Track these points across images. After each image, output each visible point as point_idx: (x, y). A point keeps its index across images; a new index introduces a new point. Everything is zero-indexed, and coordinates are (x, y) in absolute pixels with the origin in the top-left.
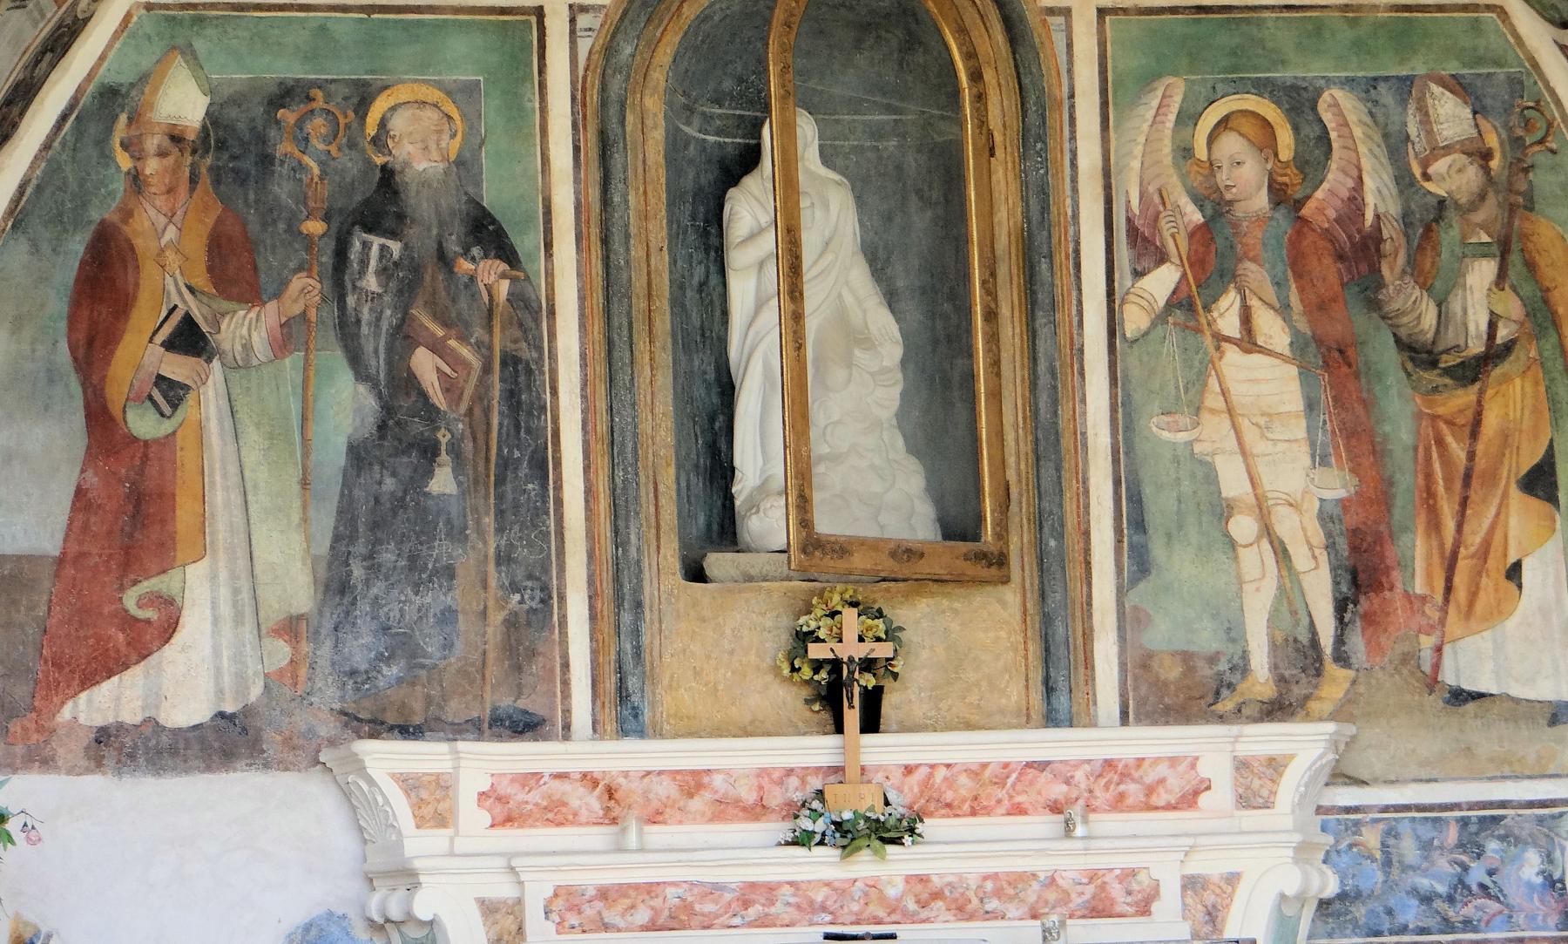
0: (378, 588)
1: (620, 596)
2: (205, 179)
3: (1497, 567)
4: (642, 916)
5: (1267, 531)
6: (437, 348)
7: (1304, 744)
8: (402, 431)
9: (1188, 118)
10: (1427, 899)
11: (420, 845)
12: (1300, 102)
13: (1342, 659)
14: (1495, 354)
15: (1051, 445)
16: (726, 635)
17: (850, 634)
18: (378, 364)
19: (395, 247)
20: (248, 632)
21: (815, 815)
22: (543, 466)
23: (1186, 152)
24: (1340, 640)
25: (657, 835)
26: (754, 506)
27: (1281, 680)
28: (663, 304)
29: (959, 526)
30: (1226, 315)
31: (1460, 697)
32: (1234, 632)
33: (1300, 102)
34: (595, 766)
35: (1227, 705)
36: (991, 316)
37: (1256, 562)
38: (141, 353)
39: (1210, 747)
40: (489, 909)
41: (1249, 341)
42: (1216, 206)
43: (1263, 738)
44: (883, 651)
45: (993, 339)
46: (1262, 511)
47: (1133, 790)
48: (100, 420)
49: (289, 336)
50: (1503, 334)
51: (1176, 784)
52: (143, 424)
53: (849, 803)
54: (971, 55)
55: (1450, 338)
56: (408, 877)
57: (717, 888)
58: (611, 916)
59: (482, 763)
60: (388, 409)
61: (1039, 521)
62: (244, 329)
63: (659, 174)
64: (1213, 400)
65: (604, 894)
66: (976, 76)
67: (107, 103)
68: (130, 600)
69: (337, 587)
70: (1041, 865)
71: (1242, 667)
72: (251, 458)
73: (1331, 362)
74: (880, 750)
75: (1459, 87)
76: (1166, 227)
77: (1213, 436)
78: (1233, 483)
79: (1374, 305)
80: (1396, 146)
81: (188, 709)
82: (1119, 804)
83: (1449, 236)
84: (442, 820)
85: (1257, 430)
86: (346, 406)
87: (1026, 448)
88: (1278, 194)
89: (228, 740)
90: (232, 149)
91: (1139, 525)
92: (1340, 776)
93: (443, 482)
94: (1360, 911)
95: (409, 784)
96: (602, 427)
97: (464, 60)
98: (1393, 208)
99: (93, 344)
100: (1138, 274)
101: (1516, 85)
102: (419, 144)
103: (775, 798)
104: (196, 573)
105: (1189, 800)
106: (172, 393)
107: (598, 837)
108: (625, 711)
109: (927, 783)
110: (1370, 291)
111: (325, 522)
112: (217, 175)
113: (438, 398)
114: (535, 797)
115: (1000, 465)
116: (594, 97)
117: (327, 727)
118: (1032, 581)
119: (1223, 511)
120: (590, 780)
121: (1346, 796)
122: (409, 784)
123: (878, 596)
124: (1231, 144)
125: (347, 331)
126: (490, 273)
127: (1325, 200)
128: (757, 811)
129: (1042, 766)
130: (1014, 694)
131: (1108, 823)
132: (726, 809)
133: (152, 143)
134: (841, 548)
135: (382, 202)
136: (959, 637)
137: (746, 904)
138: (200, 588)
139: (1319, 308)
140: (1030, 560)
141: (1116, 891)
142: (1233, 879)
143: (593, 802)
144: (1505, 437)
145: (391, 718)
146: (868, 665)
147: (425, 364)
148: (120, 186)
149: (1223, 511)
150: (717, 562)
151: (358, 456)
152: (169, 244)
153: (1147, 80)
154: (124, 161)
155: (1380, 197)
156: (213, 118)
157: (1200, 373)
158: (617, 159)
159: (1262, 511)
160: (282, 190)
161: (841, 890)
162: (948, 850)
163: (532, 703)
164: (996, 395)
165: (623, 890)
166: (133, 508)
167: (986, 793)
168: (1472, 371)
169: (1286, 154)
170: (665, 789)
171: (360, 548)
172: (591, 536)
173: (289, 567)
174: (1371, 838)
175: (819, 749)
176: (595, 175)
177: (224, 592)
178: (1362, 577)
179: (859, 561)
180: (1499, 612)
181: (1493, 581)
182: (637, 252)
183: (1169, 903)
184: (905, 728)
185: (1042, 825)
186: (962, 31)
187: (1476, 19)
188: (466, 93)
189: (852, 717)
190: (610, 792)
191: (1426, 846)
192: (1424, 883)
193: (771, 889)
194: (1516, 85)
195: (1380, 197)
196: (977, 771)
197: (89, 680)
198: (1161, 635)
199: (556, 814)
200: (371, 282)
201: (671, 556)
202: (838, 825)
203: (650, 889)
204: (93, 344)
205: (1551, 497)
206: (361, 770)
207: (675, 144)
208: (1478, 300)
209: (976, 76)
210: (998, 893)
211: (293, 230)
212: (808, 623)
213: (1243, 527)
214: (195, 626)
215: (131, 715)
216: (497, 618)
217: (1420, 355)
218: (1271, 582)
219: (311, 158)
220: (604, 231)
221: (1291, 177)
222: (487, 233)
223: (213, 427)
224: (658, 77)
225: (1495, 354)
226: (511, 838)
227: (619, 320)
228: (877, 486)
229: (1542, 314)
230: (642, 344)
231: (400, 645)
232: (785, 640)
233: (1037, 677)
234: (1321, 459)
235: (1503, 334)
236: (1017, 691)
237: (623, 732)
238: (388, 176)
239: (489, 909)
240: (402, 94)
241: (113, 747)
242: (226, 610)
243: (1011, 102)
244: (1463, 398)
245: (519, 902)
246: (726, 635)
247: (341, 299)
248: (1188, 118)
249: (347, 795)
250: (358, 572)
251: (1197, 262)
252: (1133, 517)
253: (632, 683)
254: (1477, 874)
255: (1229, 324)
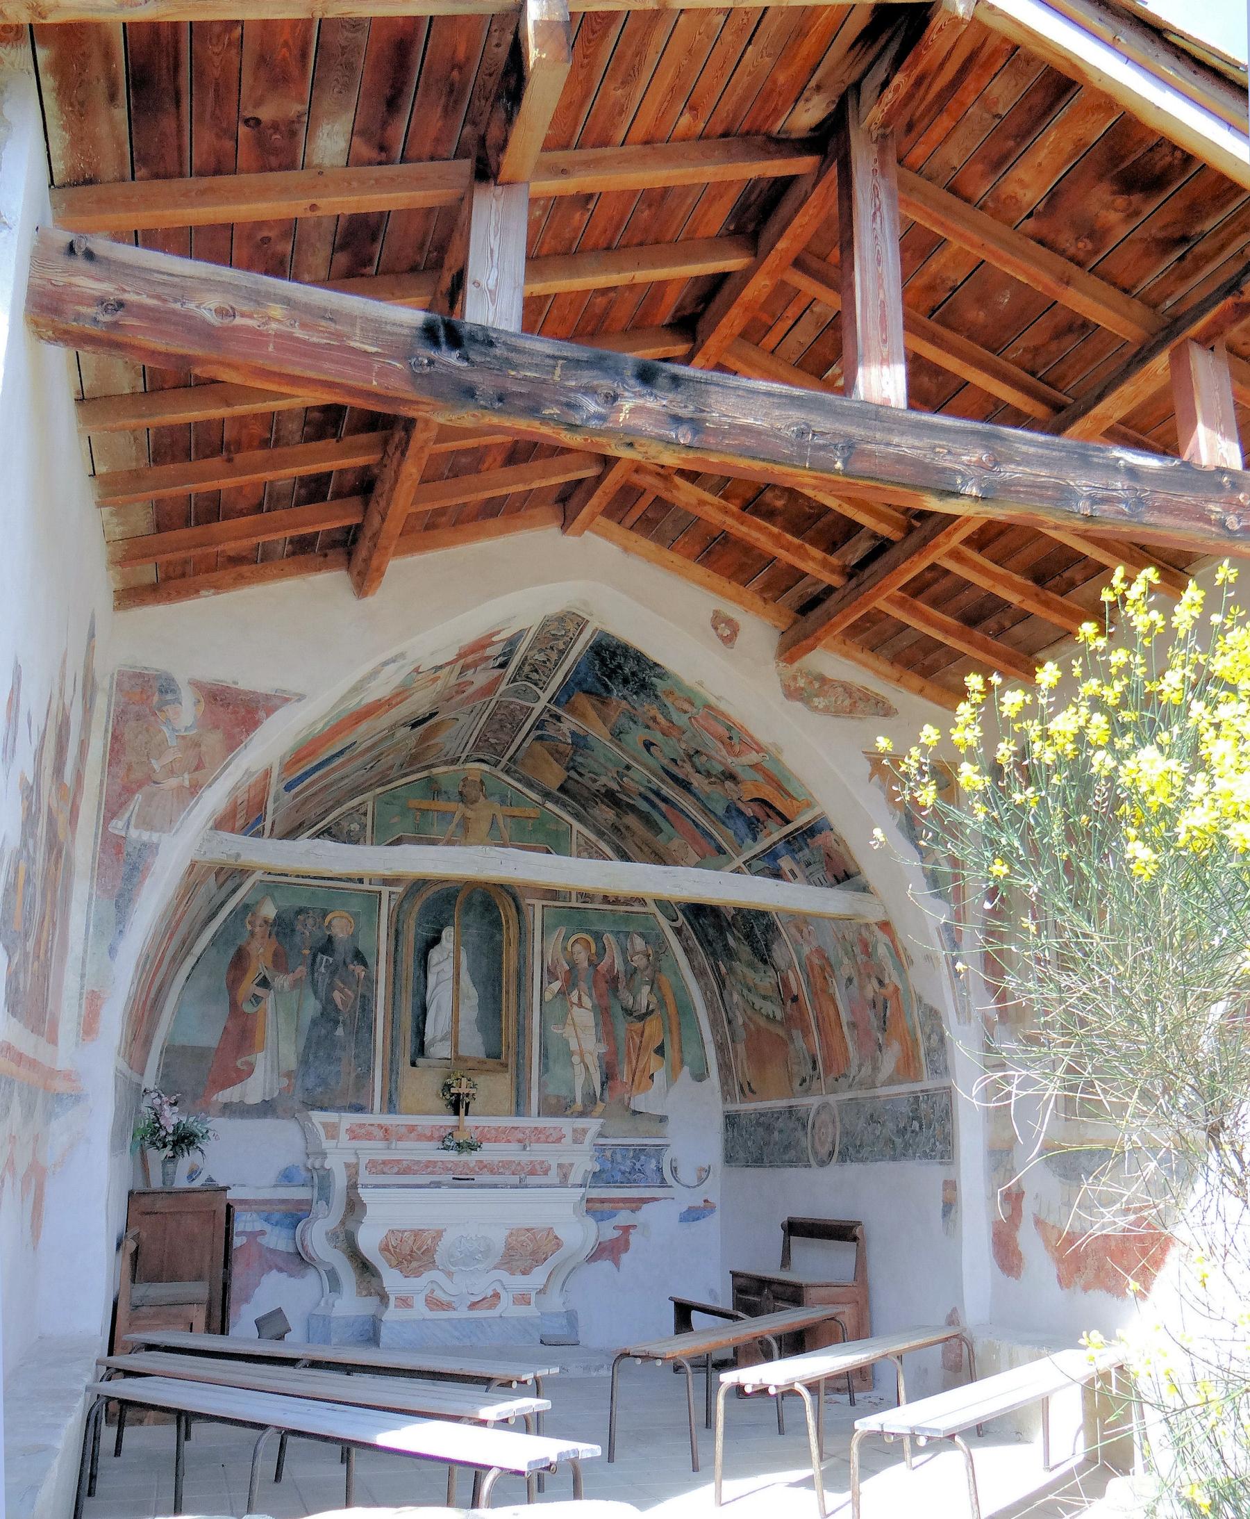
0: (317, 1063)
1: (392, 1070)
2: (273, 936)
3: (647, 1075)
4: (396, 1169)
5: (583, 1061)
6: (341, 991)
7: (592, 1125)
8: (329, 1015)
9: (566, 938)
10: (623, 1173)
11: (327, 1144)
12: (598, 936)
13: (602, 1100)
14: (649, 1013)
15: (522, 1032)
16: (422, 1084)
17: (464, 1085)
18: (323, 994)
19: (331, 960)
20: (275, 1076)
21: (451, 1141)
22: (371, 1029)
23: (566, 949)
24: (602, 1094)
25: (401, 1144)
26: (432, 1044)
27: (585, 1106)
28: (411, 982)
29: (494, 1055)
30: (574, 997)
31: (635, 1113)
32: (572, 1090)
33: (598, 936)
34: (382, 1122)
35: (568, 1112)
36: (507, 992)
37: (579, 1069)
38: (249, 986)
39: (566, 1124)
40: (347, 1166)
41: (580, 1005)
42: (573, 966)
43: (581, 1123)
44: (473, 1091)
45: (508, 999)
46: (582, 1056)
47: (543, 1137)
48: (234, 1006)
49: (295, 984)
50: (651, 1007)
51: (555, 1136)
52: (248, 1008)
53: (461, 1137)
54: (506, 916)
55: (637, 1007)
56: (324, 1155)
57: (419, 1162)
58: (385, 1170)
59: (348, 1120)
60: (324, 1008)
61: (518, 1054)
62: (282, 981)
63: (412, 944)
64: (569, 1021)
65: (384, 1162)
66: (507, 922)
67: (246, 909)
68: (239, 1063)
69: (304, 1062)
70: (516, 1159)
71: (574, 1101)
72: (281, 1021)
73: (603, 1013)
74: (469, 1121)
75: (642, 935)
76: (558, 970)
77: (568, 1032)
78: (574, 1046)
79: (616, 997)
80: (624, 951)
81: (254, 1098)
82: (538, 1141)
83: (638, 977)
84: (333, 1138)
85: (581, 1029)
86: (312, 1007)
87: (515, 1032)
88: (591, 963)
89: (266, 1109)
90: (283, 927)
91: (546, 1057)
92: (601, 1135)
93: (340, 1032)
94: (604, 1176)
95: (325, 1125)
96: (390, 1017)
97: (356, 905)
98: (622, 969)
99: (234, 984)
100: (550, 983)
101: (658, 936)
102: (340, 928)
103: (436, 1135)
104: (260, 1056)
105: (559, 1140)
106: (257, 999)
107: (381, 1144)
108: (390, 1105)
109: (482, 1132)
110: (615, 990)
111: (302, 1042)
112: (277, 934)
113: (340, 1007)
114: (363, 1131)
115: (507, 1038)
116: (394, 919)
117: (297, 1106)
118: (514, 1073)
119: (571, 1054)
120: (380, 1126)
121: (602, 1141)
122: (325, 1125)
123: (469, 1073)
124: (578, 947)
125: (314, 984)
126: (359, 970)
127: (603, 966)
128: (431, 1138)
129: (516, 1128)
130: (507, 1105)
131: (535, 1146)
132: (421, 1137)
133: (258, 922)
134: (465, 1060)
135: (328, 946)
136: (491, 1088)
137: (427, 1167)
138: (261, 1061)
139: (600, 996)
140: (514, 1066)
141: (538, 1167)
142: (572, 1165)
143: (379, 1133)
144: (651, 1037)
145: (318, 1104)
146: (468, 1095)
147: (337, 995)
148: (247, 934)
149: (571, 1054)
150: (420, 1061)
151: (314, 1022)
152: (261, 953)
153: (556, 927)
154: (249, 927)
155: (619, 965)
156: (278, 916)
157: (568, 1012)
158: (401, 937)
159: (582, 1056)
160: (297, 939)
161: (456, 1164)
162: (490, 1153)
163: (362, 1102)
164: (507, 1016)
165: (390, 1162)
166: (242, 1035)
167: (500, 1135)
168: (642, 1018)
169: (593, 951)
170: (403, 1130)
171: (313, 1051)
172: (383, 1051)
173: (290, 1055)
174: (608, 1154)
175: (451, 1120)
176: (393, 942)
177: (269, 1063)
178: (609, 1076)
179: (470, 1064)
180: (647, 1088)
181: (646, 1079)
182: (404, 966)
183: (554, 1171)
184: (475, 1115)
185: (515, 1146)
186: (504, 909)
187: (429, 779)
188: (356, 915)
189: (462, 1111)
190: (386, 1130)
191: (624, 1157)
192: (623, 1168)
193: (435, 1162)
194: (658, 936)
195: (619, 965)
196: (496, 1129)
197: (224, 1087)
198: (551, 1090)
199: (369, 1136)
200: (323, 970)
201: (408, 1060)
202: (459, 1144)
203: (398, 1161)
204: (234, 984)
205: (663, 1055)
206: (310, 1120)
207: (417, 934)
208: (645, 997)
209: (507, 922)
210: (503, 1167)
211: (299, 952)
212: (449, 1081)
213: (576, 1059)
214: (259, 1073)
215: (235, 1100)
216: (353, 1075)
217: (628, 1012)
218: (582, 1077)
219: (307, 931)
220: (395, 960)
221: (594, 958)
222: (359, 957)
223: (269, 1011)
224: (414, 915)
225: (649, 1013)
226: (356, 1144)
227: (398, 986)
228: (473, 1044)
229: (662, 1003)
230: (404, 995)
231: (323, 1081)
232: (440, 1086)
233: (514, 1100)
234: (598, 1040)
235: (651, 1007)
236: (507, 1105)
237: (390, 1112)
238: (330, 939)
239: (347, 1166)
240: (336, 914)
241: (229, 1110)
242: (269, 1067)
243: (517, 931)
244: (640, 1025)
245: (357, 1164)
246: (422, 1084)
247: (313, 974)
248: (566, 938)
249: (303, 1129)
250: (311, 1058)
251: (566, 981)
252: (544, 1054)
253: (394, 1097)
254: (638, 1166)
255: (575, 999)
